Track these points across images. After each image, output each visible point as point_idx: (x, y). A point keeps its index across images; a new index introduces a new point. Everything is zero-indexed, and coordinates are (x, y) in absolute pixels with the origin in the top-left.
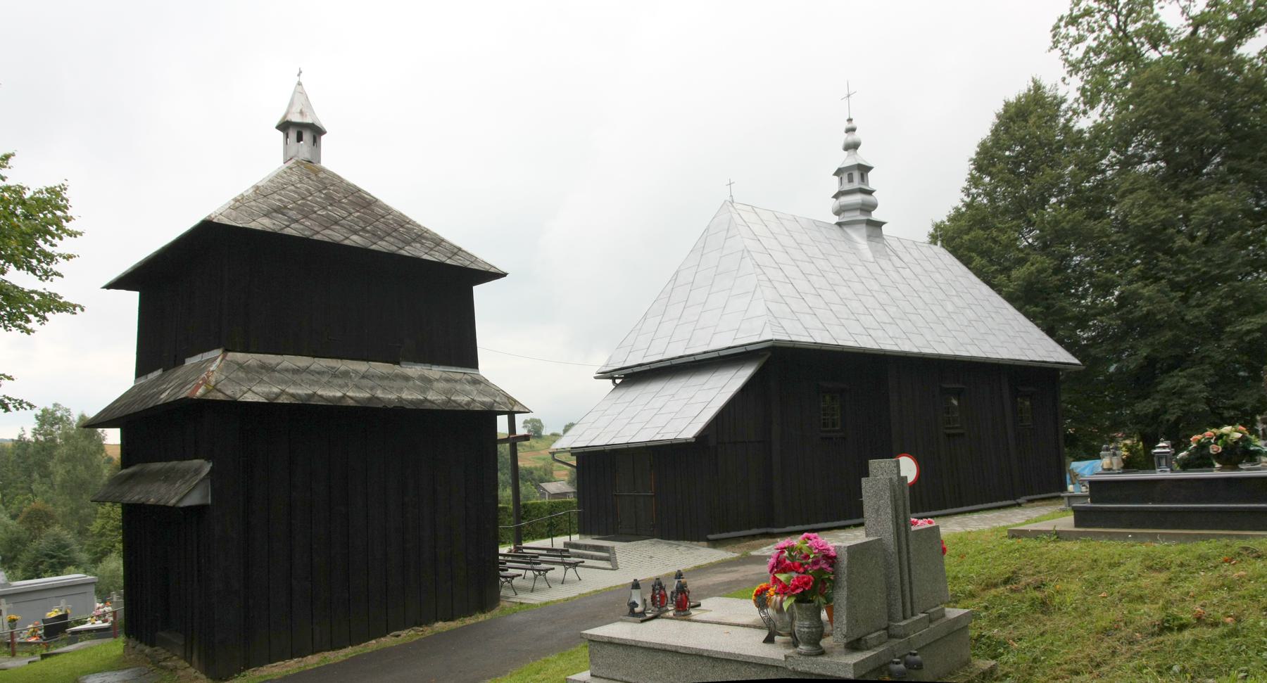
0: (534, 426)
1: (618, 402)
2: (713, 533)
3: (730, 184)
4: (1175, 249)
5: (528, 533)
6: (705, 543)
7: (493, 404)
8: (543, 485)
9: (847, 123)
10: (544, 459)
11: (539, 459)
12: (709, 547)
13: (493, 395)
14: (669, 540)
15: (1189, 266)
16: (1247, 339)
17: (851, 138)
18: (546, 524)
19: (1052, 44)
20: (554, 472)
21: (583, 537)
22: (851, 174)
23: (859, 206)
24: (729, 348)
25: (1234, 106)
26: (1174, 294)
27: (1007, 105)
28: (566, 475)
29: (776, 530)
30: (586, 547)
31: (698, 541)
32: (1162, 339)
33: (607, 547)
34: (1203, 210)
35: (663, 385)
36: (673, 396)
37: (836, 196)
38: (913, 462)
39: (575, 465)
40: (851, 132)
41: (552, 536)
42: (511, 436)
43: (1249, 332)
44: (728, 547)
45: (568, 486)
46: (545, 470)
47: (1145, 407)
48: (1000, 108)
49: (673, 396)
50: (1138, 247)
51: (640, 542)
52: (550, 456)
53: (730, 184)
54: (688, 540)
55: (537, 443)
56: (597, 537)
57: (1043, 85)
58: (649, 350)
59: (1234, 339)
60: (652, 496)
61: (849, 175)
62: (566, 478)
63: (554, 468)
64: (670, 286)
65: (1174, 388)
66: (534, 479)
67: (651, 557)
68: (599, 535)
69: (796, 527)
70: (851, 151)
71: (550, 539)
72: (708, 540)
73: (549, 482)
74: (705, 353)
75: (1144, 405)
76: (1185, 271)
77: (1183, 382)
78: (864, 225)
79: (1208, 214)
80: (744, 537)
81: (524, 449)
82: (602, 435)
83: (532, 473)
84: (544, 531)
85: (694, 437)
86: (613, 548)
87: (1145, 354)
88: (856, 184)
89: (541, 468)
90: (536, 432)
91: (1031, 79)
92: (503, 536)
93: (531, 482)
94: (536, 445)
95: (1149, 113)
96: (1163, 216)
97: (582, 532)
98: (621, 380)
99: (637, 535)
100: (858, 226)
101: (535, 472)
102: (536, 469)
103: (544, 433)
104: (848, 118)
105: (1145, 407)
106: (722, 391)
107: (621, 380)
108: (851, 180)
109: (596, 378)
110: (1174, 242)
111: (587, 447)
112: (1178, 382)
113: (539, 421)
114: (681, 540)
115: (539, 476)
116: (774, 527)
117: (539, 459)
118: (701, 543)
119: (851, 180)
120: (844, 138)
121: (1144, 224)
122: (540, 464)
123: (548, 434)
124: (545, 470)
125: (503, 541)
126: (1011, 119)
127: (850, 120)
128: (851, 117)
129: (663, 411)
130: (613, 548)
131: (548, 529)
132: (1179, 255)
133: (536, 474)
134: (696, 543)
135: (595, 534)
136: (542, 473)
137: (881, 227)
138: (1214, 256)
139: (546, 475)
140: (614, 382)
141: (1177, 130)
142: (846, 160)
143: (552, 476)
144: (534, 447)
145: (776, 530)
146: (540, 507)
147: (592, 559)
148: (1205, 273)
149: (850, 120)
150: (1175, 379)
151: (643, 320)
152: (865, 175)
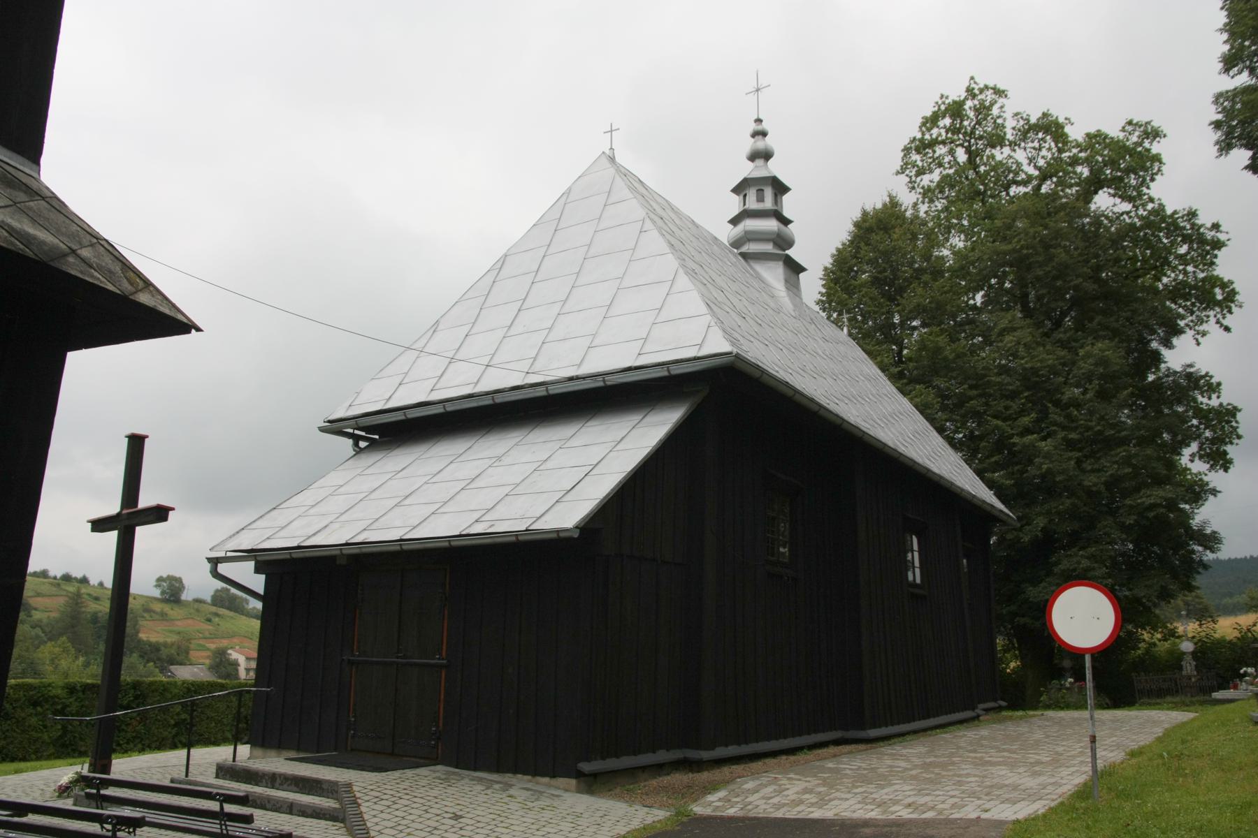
0: (171, 586)
1: (365, 472)
2: (588, 760)
3: (611, 131)
4: (1064, 401)
5: (134, 738)
6: (573, 782)
7: (65, 255)
8: (172, 667)
9: (754, 124)
10: (179, 633)
11: (171, 632)
12: (579, 791)
13: (73, 236)
14: (475, 769)
15: (1082, 422)
16: (1151, 515)
17: (760, 144)
18: (172, 722)
19: (899, 168)
20: (191, 652)
21: (259, 752)
22: (763, 190)
23: (773, 237)
24: (629, 369)
25: (1177, 216)
26: (1070, 454)
27: (865, 214)
28: (208, 657)
29: (705, 755)
30: (273, 780)
31: (554, 775)
32: (1061, 507)
33: (334, 784)
34: (1091, 361)
35: (469, 444)
36: (499, 458)
37: (735, 221)
38: (1055, 606)
39: (261, 591)
40: (760, 137)
41: (189, 745)
42: (125, 512)
43: (1152, 507)
44: (618, 790)
45: (208, 673)
46: (179, 647)
47: (1040, 592)
48: (857, 215)
49: (499, 458)
50: (1026, 394)
51: (409, 773)
52: (208, 566)
53: (611, 131)
54: (525, 773)
55: (172, 609)
56: (293, 754)
57: (900, 202)
58: (441, 380)
59: (1134, 514)
60: (441, 666)
61: (758, 190)
62: (207, 662)
63: (192, 646)
64: (490, 278)
65: (1075, 570)
66: (159, 659)
67: (456, 817)
68: (298, 749)
69: (760, 744)
70: (760, 162)
71: (185, 751)
72: (579, 775)
73: (181, 664)
74: (571, 379)
75: (1040, 589)
76: (1076, 428)
77: (1085, 563)
78: (781, 263)
79: (1096, 365)
80: (643, 768)
81: (151, 617)
82: (336, 526)
83: (158, 650)
84: (166, 734)
85: (577, 527)
86: (349, 785)
87: (1042, 525)
88: (768, 204)
89: (173, 644)
90: (172, 595)
91: (887, 194)
92: (81, 739)
93: (155, 663)
94: (170, 612)
95: (1022, 247)
96: (1051, 361)
97: (261, 741)
98: (367, 444)
99: (392, 754)
100: (772, 264)
101: (163, 648)
102: (165, 645)
103: (184, 597)
104: (756, 117)
105: (1040, 592)
106: (618, 447)
107: (367, 444)
108: (760, 199)
109: (322, 430)
110: (1063, 394)
111: (299, 547)
112: (1079, 563)
113: (179, 580)
114: (508, 771)
115: (168, 656)
116: (698, 746)
117: (171, 632)
118: (561, 781)
119: (760, 199)
120: (749, 144)
121: (1032, 368)
122: (171, 639)
123: (190, 599)
124: (179, 647)
125: (83, 749)
126: (870, 230)
127: (759, 121)
128: (761, 117)
129: (448, 508)
130: (349, 785)
131: (174, 731)
132: (1071, 408)
133: (164, 652)
134: (546, 780)
135: (289, 748)
136: (173, 652)
137: (798, 274)
138: (1106, 414)
139: (178, 654)
140: (356, 444)
141: (1050, 272)
142: (750, 169)
143: (187, 657)
144: (166, 614)
145: (705, 755)
146: (165, 690)
147: (291, 813)
148: (1100, 433)
149: (759, 121)
150: (1075, 560)
151: (432, 331)
152: (779, 197)
